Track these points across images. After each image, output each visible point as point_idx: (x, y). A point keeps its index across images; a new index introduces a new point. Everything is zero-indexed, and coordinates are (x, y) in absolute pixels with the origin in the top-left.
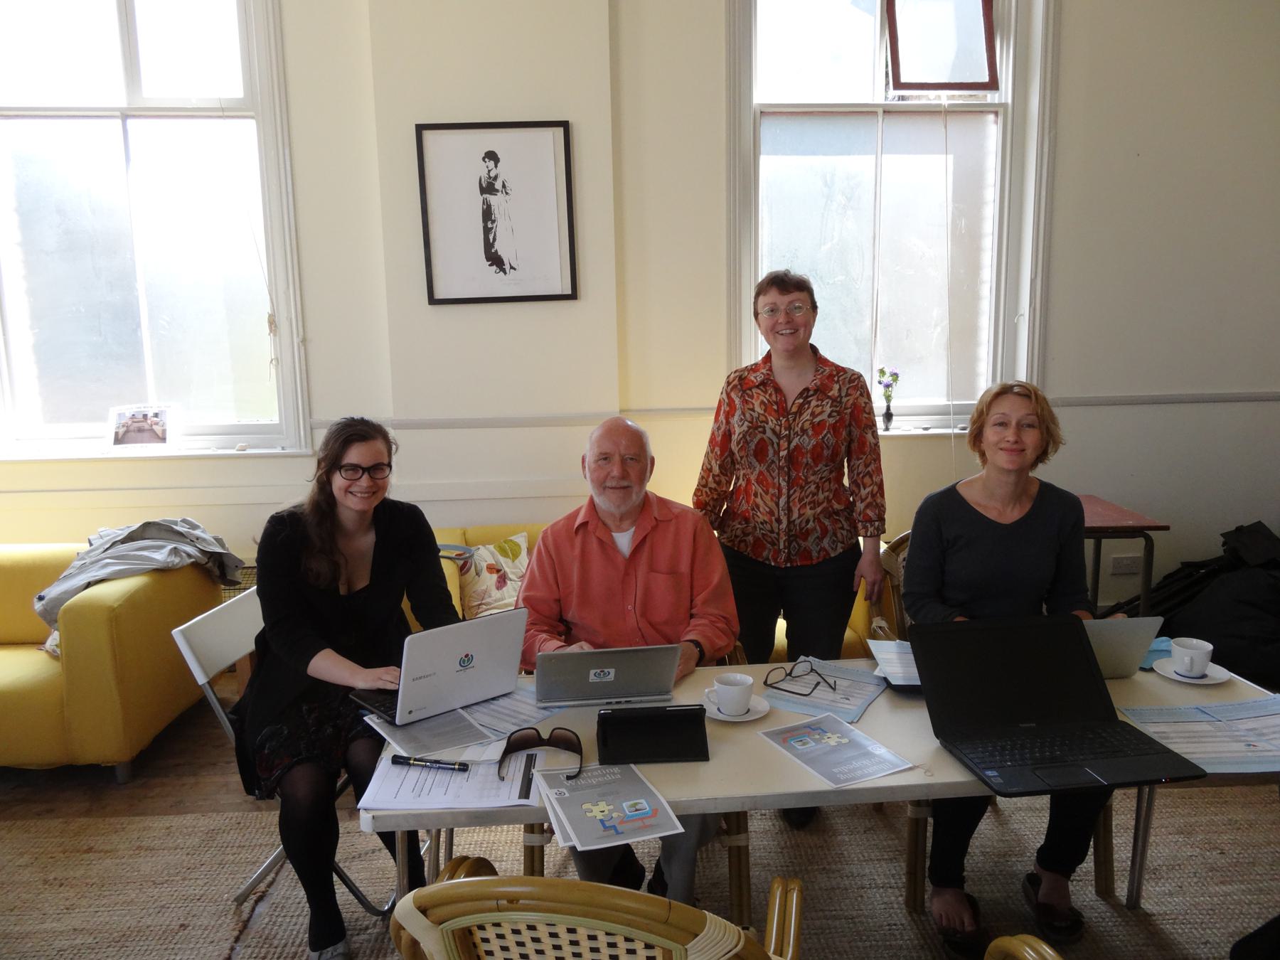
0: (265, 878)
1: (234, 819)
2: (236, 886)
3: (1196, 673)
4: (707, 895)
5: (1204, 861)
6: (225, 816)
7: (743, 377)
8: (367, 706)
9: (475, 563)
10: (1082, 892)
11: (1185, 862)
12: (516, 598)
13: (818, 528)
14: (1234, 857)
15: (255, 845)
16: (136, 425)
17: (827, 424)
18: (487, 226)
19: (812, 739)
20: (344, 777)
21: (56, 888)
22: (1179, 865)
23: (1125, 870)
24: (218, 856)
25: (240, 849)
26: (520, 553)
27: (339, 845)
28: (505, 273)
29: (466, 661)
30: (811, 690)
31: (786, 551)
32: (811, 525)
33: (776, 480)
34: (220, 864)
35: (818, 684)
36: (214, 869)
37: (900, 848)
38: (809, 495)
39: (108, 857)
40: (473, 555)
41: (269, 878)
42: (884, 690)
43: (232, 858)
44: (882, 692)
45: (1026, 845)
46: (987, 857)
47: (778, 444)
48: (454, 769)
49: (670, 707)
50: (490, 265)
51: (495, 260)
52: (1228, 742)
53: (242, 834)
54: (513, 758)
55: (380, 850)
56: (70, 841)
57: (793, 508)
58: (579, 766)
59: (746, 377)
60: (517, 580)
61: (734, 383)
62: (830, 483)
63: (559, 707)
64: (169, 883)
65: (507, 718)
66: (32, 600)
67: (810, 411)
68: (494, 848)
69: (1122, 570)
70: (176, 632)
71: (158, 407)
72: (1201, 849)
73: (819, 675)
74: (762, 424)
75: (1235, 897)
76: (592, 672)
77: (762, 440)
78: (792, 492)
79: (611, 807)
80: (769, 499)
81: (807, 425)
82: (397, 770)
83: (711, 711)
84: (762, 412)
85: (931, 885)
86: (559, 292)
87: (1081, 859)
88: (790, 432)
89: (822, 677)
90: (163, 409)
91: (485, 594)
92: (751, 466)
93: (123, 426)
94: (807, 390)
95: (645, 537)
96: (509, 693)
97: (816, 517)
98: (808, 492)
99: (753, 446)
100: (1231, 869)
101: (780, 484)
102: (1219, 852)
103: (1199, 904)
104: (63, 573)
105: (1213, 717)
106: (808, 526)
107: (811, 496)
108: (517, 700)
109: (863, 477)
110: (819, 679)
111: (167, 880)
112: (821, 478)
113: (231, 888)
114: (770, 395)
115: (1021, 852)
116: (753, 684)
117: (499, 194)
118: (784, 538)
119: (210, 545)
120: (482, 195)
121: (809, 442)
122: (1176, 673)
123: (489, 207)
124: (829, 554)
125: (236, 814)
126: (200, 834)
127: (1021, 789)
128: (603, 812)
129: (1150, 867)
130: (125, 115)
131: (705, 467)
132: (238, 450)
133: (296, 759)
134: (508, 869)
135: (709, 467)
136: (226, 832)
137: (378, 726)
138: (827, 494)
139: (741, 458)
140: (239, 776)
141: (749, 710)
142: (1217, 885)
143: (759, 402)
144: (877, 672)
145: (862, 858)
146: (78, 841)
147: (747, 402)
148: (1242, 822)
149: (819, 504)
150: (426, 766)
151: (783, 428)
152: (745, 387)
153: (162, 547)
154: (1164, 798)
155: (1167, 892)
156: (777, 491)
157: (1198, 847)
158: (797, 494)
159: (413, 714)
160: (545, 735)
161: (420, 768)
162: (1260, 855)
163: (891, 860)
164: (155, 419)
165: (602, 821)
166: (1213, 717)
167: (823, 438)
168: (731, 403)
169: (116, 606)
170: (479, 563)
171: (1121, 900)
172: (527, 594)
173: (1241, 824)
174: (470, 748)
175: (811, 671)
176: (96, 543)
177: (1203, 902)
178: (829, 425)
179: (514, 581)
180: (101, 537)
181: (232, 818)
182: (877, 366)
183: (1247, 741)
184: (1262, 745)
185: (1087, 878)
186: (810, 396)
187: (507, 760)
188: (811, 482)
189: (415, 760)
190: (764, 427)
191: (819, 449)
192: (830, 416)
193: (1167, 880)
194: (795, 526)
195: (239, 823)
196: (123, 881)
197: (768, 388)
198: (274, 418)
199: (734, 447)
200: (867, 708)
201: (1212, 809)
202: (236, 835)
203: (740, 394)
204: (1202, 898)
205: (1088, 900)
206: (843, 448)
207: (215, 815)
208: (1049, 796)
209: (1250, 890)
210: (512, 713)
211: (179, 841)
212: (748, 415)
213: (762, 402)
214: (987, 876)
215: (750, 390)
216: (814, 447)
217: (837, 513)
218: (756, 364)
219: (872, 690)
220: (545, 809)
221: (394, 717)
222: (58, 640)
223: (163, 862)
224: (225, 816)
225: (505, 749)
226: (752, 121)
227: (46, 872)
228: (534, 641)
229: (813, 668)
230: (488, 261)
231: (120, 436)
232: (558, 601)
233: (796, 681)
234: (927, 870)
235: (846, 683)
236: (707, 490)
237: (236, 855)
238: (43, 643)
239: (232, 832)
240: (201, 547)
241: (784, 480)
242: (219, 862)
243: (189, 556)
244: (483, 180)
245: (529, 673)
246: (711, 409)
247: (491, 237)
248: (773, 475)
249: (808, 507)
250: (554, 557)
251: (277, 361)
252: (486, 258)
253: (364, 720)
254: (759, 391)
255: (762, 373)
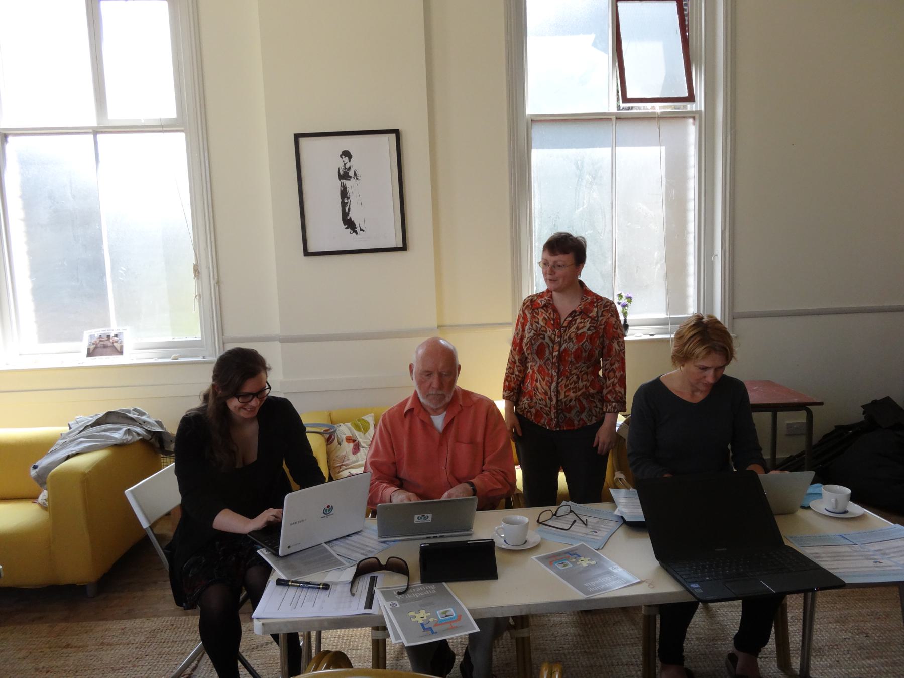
0: (190, 664)
1: (169, 622)
2: (171, 671)
3: (840, 509)
4: (502, 672)
5: (855, 642)
6: (163, 619)
7: (534, 300)
8: (259, 542)
9: (338, 436)
10: (768, 666)
11: (841, 643)
12: (365, 461)
13: (577, 405)
14: (875, 639)
15: (184, 641)
16: (102, 343)
17: (586, 335)
18: (344, 201)
19: (570, 562)
20: (244, 593)
21: (45, 674)
22: (837, 645)
23: (798, 650)
24: (157, 649)
25: (173, 644)
26: (369, 428)
27: (242, 640)
28: (357, 233)
29: (328, 510)
30: (570, 526)
31: (556, 420)
32: (572, 403)
33: (550, 371)
34: (159, 655)
35: (575, 521)
36: (155, 658)
37: (638, 636)
38: (572, 383)
39: (80, 651)
40: (336, 430)
41: (194, 665)
42: (622, 525)
43: (168, 650)
44: (620, 526)
45: (728, 632)
46: (700, 641)
47: (553, 347)
48: (319, 588)
49: (469, 541)
50: (346, 228)
51: (349, 223)
52: (863, 560)
53: (174, 633)
54: (361, 579)
55: (271, 643)
56: (54, 640)
57: (561, 391)
58: (407, 584)
59: (535, 300)
60: (366, 447)
61: (527, 304)
62: (587, 375)
63: (394, 541)
64: (123, 669)
65: (358, 550)
66: (29, 468)
67: (575, 326)
68: (352, 640)
69: (792, 432)
70: (127, 492)
71: (117, 330)
72: (852, 633)
73: (576, 514)
74: (543, 333)
75: (877, 668)
76: (416, 517)
77: (542, 344)
78: (560, 380)
79: (429, 614)
80: (545, 383)
81: (573, 335)
82: (280, 589)
83: (500, 542)
84: (544, 325)
85: (660, 663)
86: (394, 246)
87: (765, 642)
88: (561, 340)
89: (578, 516)
90: (121, 331)
91: (344, 458)
92: (534, 360)
93: (93, 344)
94: (574, 312)
95: (453, 419)
96: (359, 532)
97: (577, 398)
98: (571, 381)
99: (535, 347)
100: (873, 647)
101: (552, 374)
102: (865, 635)
103: (851, 674)
104: (50, 449)
105: (851, 541)
106: (571, 404)
107: (573, 384)
108: (364, 536)
109: (608, 372)
110: (576, 518)
111: (122, 667)
112: (581, 372)
113: (167, 672)
114: (550, 314)
115: (725, 638)
116: (528, 523)
117: (352, 179)
118: (554, 411)
119: (153, 426)
120: (340, 180)
121: (572, 347)
122: (826, 510)
123: (345, 188)
124: (586, 423)
125: (171, 618)
126: (145, 633)
127: (716, 597)
128: (423, 617)
129: (816, 647)
130: (96, 132)
131: (510, 360)
132: (173, 359)
133: (211, 581)
134: (361, 655)
135: (513, 360)
136: (164, 631)
137: (267, 557)
138: (585, 383)
139: (528, 354)
140: (171, 591)
141: (526, 542)
142: (863, 660)
143: (542, 318)
144: (616, 513)
145: (611, 644)
146: (59, 640)
147: (534, 317)
148: (881, 614)
149: (579, 390)
150: (300, 586)
151: (556, 337)
152: (534, 307)
153: (119, 429)
154: (822, 598)
155: (828, 665)
156: (550, 379)
157: (850, 632)
158: (564, 382)
159: (291, 548)
160: (383, 562)
161: (297, 588)
162: (894, 638)
163: (632, 644)
164: (116, 338)
165: (422, 624)
166: (851, 541)
167: (583, 344)
168: (525, 317)
169: (87, 472)
170: (340, 436)
171: (795, 671)
172: (373, 459)
173: (880, 615)
174: (331, 572)
175: (570, 512)
176: (74, 427)
177: (854, 672)
178: (588, 336)
179: (365, 448)
180: (77, 423)
181: (168, 621)
182: (617, 292)
183: (875, 559)
184: (885, 562)
185: (771, 656)
186: (576, 316)
187: (357, 582)
188: (573, 374)
189: (293, 582)
190: (544, 335)
191: (579, 351)
192: (589, 330)
193: (828, 656)
194: (562, 403)
195: (173, 625)
196: (90, 669)
197: (549, 309)
198: (198, 336)
199: (525, 348)
200: (609, 538)
201: (860, 604)
202: (170, 634)
203: (531, 312)
204: (853, 670)
205: (772, 672)
206: (597, 352)
207: (156, 619)
208: (741, 601)
209: (888, 663)
210: (361, 546)
211: (131, 638)
212: (534, 326)
213: (544, 319)
214: (700, 656)
215: (538, 309)
216: (576, 350)
217: (592, 396)
218: (543, 292)
219: (613, 525)
220: (382, 616)
221: (277, 551)
222: (47, 495)
223: (119, 654)
224: (163, 619)
225: (356, 573)
226: (525, 128)
227: (37, 662)
228: (378, 489)
229: (572, 510)
230: (344, 225)
231: (91, 351)
232: (394, 463)
233: (560, 519)
234: (657, 651)
235: (595, 520)
236: (514, 376)
237: (170, 648)
238: (37, 498)
239: (168, 631)
240: (146, 428)
241: (555, 371)
242: (158, 653)
243: (138, 434)
244: (341, 170)
245: (374, 516)
246: (509, 324)
247: (347, 209)
248: (549, 367)
249: (571, 391)
250: (391, 433)
251: (200, 296)
252: (343, 223)
253: (257, 553)
254: (543, 311)
255: (545, 299)
